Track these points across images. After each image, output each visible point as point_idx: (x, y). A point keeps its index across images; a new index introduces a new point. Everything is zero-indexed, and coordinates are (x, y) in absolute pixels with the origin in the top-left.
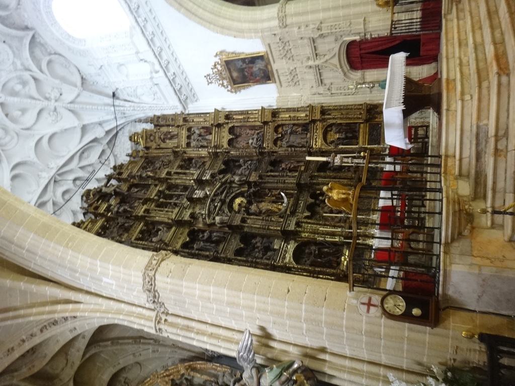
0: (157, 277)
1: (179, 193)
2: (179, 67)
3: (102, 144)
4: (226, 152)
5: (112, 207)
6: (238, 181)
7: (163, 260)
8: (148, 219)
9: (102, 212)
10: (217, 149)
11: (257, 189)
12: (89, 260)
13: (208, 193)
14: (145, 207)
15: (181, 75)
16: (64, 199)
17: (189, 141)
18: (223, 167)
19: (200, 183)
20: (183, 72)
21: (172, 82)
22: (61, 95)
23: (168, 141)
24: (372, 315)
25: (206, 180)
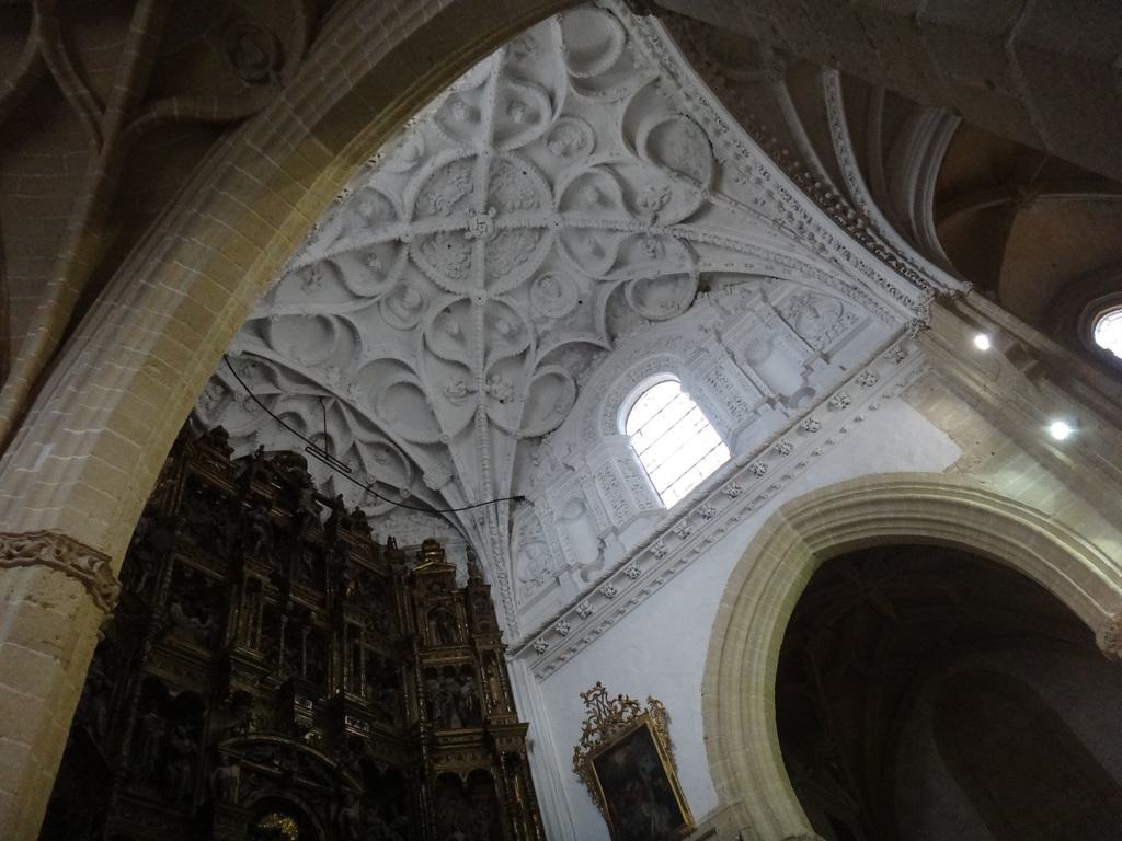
0: (34, 570)
1: (304, 660)
2: (606, 622)
3: (410, 486)
4: (423, 769)
5: (265, 509)
7: (88, 585)
8: (234, 591)
9: (252, 487)
10: (427, 745)
12: (108, 410)
13: (307, 737)
14: (265, 580)
15: (588, 629)
16: (284, 415)
17: (440, 672)
18: (382, 770)
19: (332, 714)
20: (597, 633)
21: (569, 611)
22: (501, 401)
23: (433, 623)
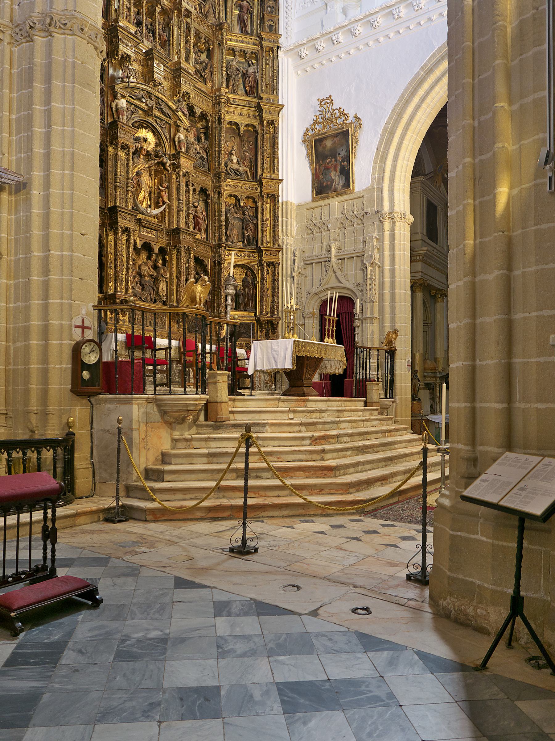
6: (179, 138)
11: (169, 168)
19: (176, 73)
24: (73, 332)
25: (179, 85)
